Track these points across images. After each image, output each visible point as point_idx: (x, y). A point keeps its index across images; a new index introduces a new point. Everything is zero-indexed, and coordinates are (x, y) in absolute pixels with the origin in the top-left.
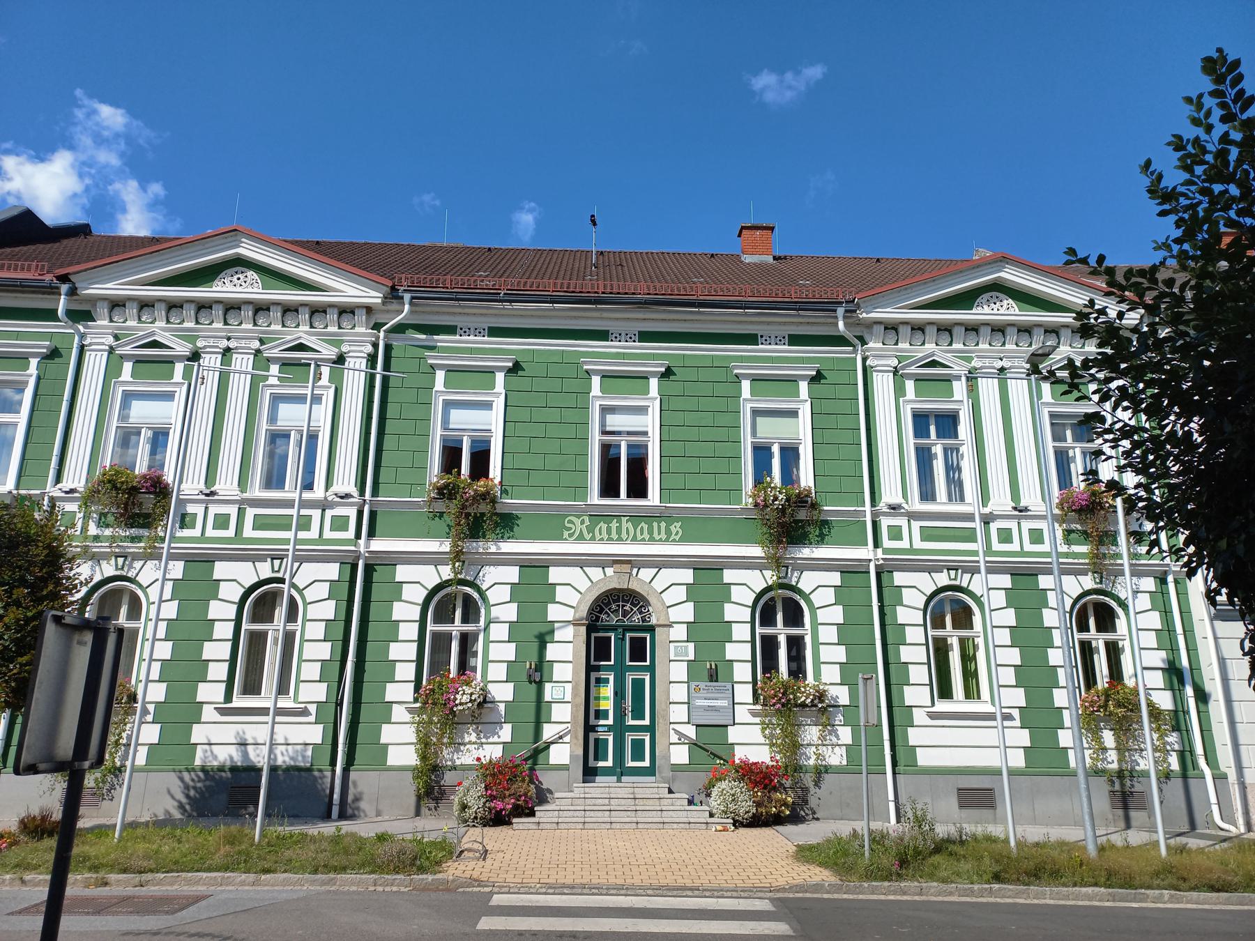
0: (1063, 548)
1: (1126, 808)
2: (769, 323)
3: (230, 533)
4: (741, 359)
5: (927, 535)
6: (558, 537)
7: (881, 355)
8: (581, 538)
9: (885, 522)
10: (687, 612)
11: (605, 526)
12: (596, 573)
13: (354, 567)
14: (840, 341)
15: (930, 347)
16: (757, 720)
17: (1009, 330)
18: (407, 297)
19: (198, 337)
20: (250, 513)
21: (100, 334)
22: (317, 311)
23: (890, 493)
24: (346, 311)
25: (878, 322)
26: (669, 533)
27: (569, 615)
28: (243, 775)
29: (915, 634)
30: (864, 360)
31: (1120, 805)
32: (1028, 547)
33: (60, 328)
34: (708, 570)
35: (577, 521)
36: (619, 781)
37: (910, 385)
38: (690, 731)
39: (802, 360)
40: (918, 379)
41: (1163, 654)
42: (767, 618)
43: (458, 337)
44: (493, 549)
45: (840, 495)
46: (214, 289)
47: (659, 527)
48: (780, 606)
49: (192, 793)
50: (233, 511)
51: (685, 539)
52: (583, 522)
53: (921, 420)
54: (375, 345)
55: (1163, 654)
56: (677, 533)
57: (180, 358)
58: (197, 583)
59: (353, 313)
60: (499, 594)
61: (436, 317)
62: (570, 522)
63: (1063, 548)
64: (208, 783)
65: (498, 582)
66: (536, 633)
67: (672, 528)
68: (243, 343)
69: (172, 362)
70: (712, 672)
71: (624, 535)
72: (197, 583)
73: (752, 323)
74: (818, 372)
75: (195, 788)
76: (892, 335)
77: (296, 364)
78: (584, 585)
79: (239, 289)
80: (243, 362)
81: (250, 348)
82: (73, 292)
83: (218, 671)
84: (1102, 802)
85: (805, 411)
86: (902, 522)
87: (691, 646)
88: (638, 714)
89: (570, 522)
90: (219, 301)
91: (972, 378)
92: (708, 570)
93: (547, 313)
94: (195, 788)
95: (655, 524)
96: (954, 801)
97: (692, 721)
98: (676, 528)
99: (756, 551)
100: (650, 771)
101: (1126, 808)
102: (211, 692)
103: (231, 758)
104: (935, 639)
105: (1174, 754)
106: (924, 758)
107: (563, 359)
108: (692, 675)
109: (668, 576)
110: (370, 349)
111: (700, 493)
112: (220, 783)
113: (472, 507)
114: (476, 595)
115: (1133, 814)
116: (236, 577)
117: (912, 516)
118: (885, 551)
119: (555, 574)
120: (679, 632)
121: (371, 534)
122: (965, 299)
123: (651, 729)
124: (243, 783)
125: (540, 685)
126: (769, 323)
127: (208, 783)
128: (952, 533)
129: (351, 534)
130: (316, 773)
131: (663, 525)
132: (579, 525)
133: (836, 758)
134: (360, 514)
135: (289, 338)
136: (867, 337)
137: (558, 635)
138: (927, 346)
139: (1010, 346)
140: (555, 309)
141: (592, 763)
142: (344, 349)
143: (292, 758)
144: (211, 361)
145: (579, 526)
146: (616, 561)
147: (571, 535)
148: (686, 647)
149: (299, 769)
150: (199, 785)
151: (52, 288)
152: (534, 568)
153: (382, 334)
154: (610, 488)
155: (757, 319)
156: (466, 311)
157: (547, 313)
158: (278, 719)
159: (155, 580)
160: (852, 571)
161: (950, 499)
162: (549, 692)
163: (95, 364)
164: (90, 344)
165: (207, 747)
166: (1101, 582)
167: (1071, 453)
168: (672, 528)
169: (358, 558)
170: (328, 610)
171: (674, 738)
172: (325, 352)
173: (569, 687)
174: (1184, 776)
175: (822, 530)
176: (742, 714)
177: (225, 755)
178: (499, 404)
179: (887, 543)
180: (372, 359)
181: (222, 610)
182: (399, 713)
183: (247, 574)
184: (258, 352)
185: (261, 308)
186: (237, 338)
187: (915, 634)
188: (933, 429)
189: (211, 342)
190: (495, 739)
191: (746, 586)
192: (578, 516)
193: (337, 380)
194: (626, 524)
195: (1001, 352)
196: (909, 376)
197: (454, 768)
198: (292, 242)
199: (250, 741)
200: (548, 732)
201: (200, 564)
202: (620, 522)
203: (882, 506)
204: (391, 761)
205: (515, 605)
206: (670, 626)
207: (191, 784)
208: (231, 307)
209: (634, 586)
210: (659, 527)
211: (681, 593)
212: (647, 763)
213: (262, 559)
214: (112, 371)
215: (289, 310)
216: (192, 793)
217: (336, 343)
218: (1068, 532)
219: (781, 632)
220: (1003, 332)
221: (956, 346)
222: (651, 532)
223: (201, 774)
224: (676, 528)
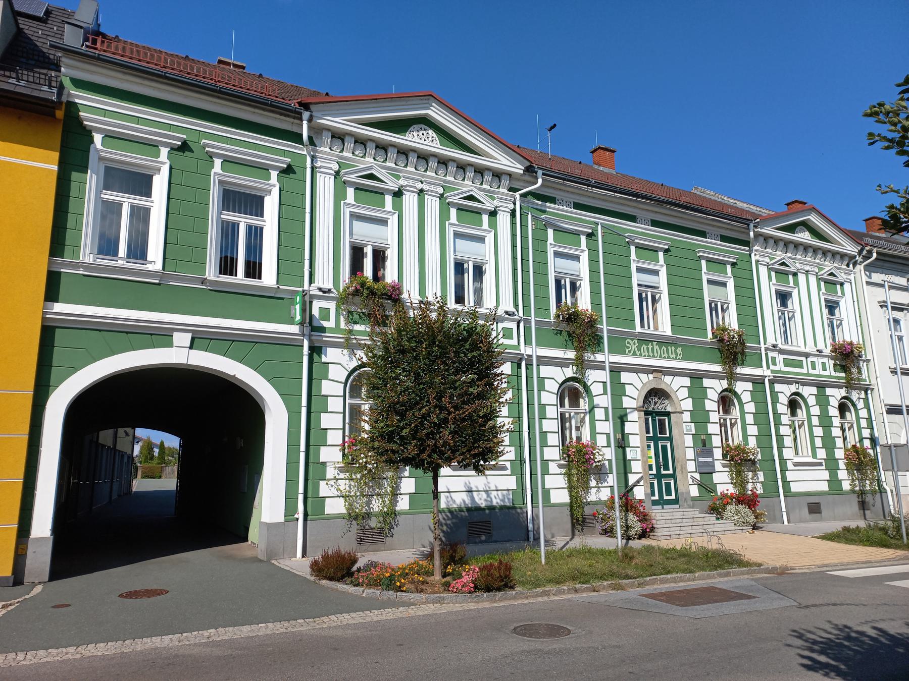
0: (833, 374)
1: (864, 510)
5: (787, 363)
6: (623, 353)
7: (328, 157)
8: (634, 354)
11: (650, 347)
12: (644, 377)
13: (519, 366)
15: (369, 160)
16: (728, 469)
17: (468, 169)
18: (540, 172)
22: (480, 171)
24: (498, 175)
25: (328, 129)
28: (475, 513)
29: (335, 404)
32: (811, 372)
34: (696, 377)
35: (632, 343)
36: (663, 508)
40: (358, 188)
44: (592, 358)
49: (445, 528)
51: (685, 358)
61: (608, 204)
63: (833, 374)
64: (454, 520)
65: (596, 378)
66: (618, 415)
68: (432, 188)
74: (289, 166)
75: (446, 524)
80: (432, 205)
81: (436, 192)
84: (855, 507)
85: (731, 284)
86: (775, 354)
87: (693, 425)
88: (667, 468)
91: (398, 194)
92: (696, 377)
93: (610, 199)
94: (446, 524)
96: (806, 510)
99: (718, 368)
100: (676, 502)
101: (864, 510)
103: (464, 502)
104: (352, 407)
106: (795, 488)
110: (512, 207)
112: (462, 519)
114: (581, 389)
115: (867, 512)
117: (782, 352)
118: (772, 371)
120: (687, 417)
122: (400, 126)
123: (673, 476)
124: (475, 520)
125: (624, 449)
126: (713, 226)
127: (454, 520)
129: (514, 342)
130: (519, 511)
135: (464, 189)
137: (630, 417)
138: (367, 159)
139: (410, 169)
140: (563, 184)
143: (501, 500)
144: (410, 201)
149: (509, 508)
150: (449, 522)
151: (296, 112)
152: (615, 371)
154: (227, 265)
155: (622, 201)
156: (568, 189)
157: (610, 199)
160: (758, 382)
162: (630, 453)
164: (320, 167)
165: (448, 494)
166: (576, 373)
167: (466, 266)
169: (521, 359)
171: (690, 482)
172: (487, 204)
173: (639, 450)
174: (881, 493)
176: (718, 466)
177: (460, 499)
179: (772, 367)
181: (711, 405)
182: (553, 467)
184: (442, 195)
186: (428, 183)
187: (335, 404)
190: (605, 484)
191: (714, 387)
192: (632, 340)
195: (423, 176)
196: (351, 184)
197: (588, 503)
199: (474, 489)
200: (632, 479)
204: (328, 510)
207: (443, 521)
209: (663, 387)
212: (673, 497)
215: (462, 167)
216: (445, 528)
218: (835, 365)
220: (446, 165)
221: (484, 186)
223: (449, 514)
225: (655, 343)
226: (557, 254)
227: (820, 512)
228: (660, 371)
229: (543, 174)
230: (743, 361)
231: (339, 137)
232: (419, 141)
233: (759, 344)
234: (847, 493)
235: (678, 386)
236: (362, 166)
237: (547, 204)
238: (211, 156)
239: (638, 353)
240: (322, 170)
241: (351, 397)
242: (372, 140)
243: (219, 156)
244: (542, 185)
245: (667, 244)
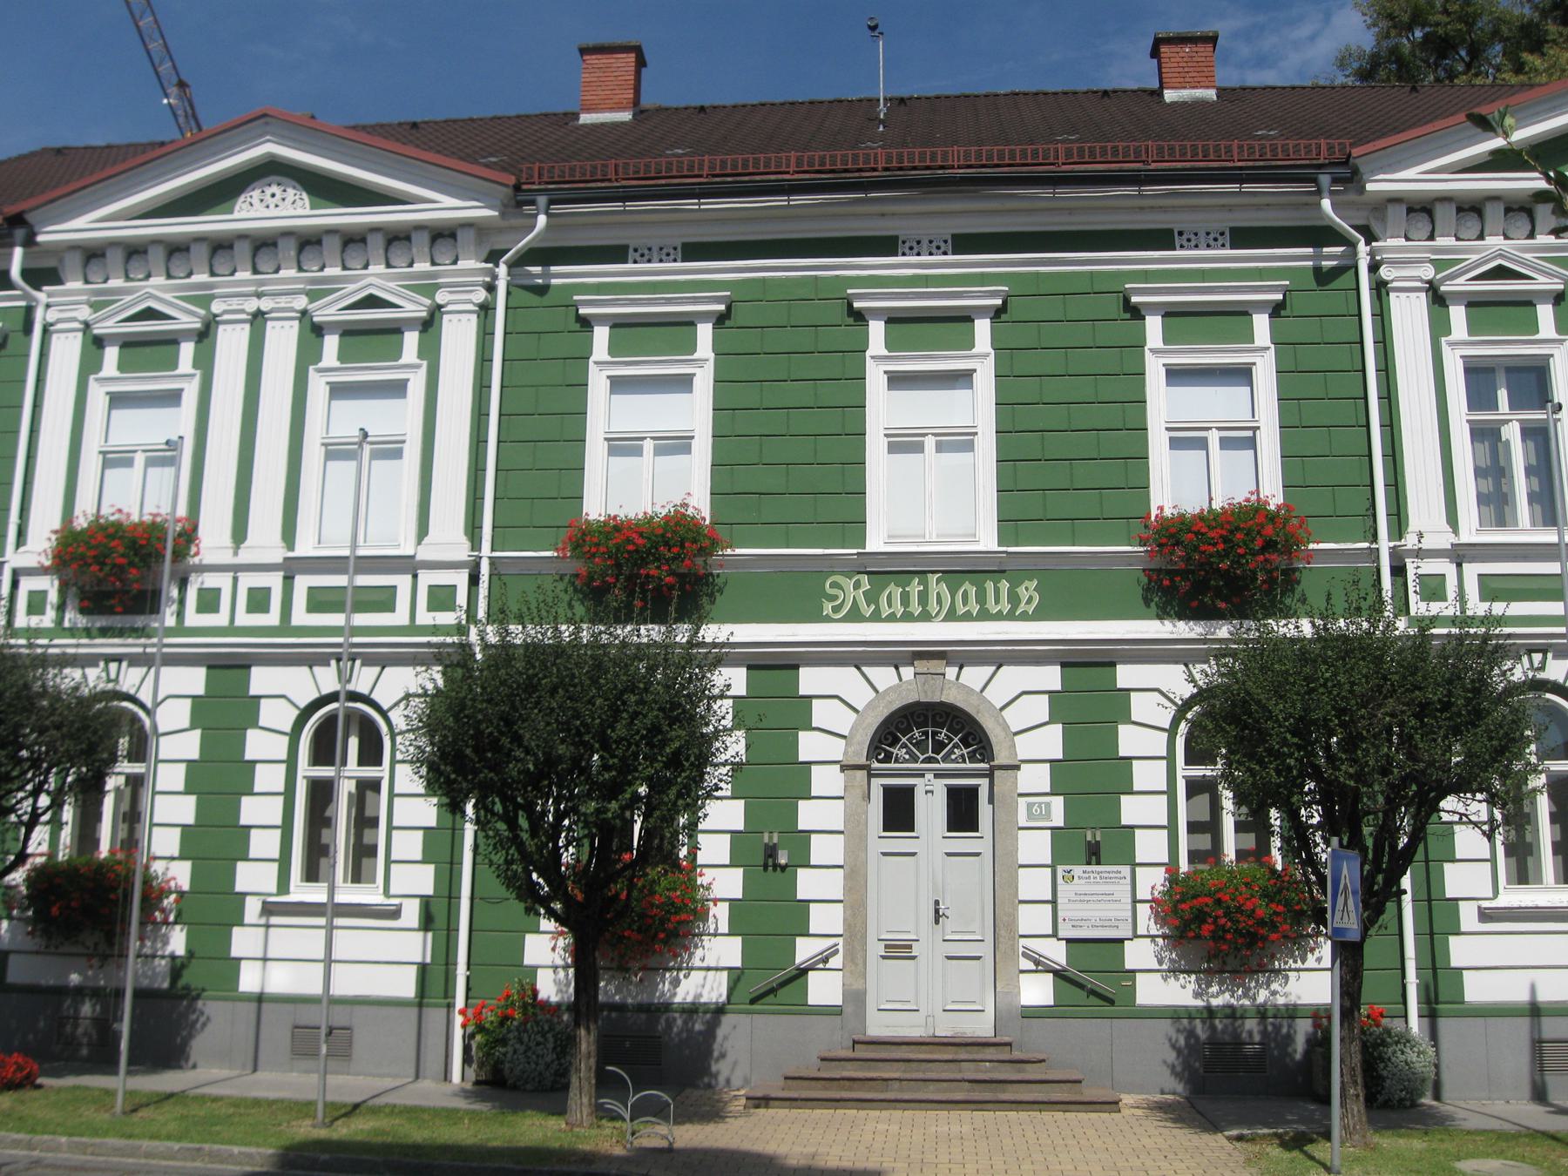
3: (272, 618)
4: (1146, 276)
6: (817, 617)
7: (1406, 259)
8: (854, 616)
10: (1051, 742)
12: (884, 677)
19: (213, 297)
20: (302, 583)
22: (397, 238)
23: (1426, 519)
24: (443, 235)
25: (1394, 199)
26: (1014, 599)
27: (836, 749)
30: (1374, 268)
35: (849, 584)
37: (1458, 314)
38: (1057, 953)
39: (1260, 274)
40: (1475, 303)
42: (324, 751)
43: (629, 266)
45: (1337, 523)
46: (236, 215)
47: (997, 591)
50: (274, 581)
52: (857, 586)
53: (1479, 375)
54: (491, 288)
56: (1030, 601)
57: (410, 323)
58: (226, 710)
59: (408, 238)
60: (173, 715)
62: (834, 585)
67: (1021, 590)
68: (283, 302)
71: (933, 607)
72: (226, 710)
76: (1473, 225)
77: (371, 336)
79: (273, 212)
80: (283, 340)
81: (292, 310)
83: (265, 844)
89: (834, 585)
90: (242, 236)
95: (990, 586)
97: (1061, 934)
98: (1028, 590)
106: (1476, 990)
107: (1093, 287)
108: (1061, 853)
109: (1014, 678)
110: (481, 295)
111: (1073, 527)
116: (283, 692)
119: (1126, 675)
120: (1035, 778)
126: (1174, 208)
128: (1534, 584)
131: (1005, 585)
132: (852, 590)
136: (1376, 228)
144: (232, 343)
145: (851, 593)
147: (836, 609)
148: (1048, 805)
152: (775, 667)
153: (502, 270)
155: (1293, 199)
158: (339, 921)
159: (171, 698)
161: (1533, 524)
163: (66, 352)
168: (1021, 590)
178: (704, 380)
183: (303, 685)
185: (308, 242)
188: (1503, 395)
189: (235, 303)
194: (936, 586)
196: (1458, 297)
198: (354, 128)
201: (228, 670)
202: (925, 583)
203: (1410, 541)
205: (198, 732)
208: (263, 245)
209: (951, 696)
210: (997, 591)
211: (1039, 708)
213: (323, 661)
214: (308, 354)
215: (353, 240)
217: (430, 290)
219: (352, 770)
222: (981, 598)
224: (1028, 590)
225: (933, 578)
226: (1176, 375)
228: (941, 656)
229: (1335, 181)
231: (92, 255)
232: (267, 213)
233: (1375, 538)
236: (1474, 257)
237: (554, 269)
238: (586, 323)
239: (868, 611)
240: (59, 326)
241: (1190, 760)
242: (1494, 197)
243: (877, 313)
244: (548, 226)
245: (717, 300)
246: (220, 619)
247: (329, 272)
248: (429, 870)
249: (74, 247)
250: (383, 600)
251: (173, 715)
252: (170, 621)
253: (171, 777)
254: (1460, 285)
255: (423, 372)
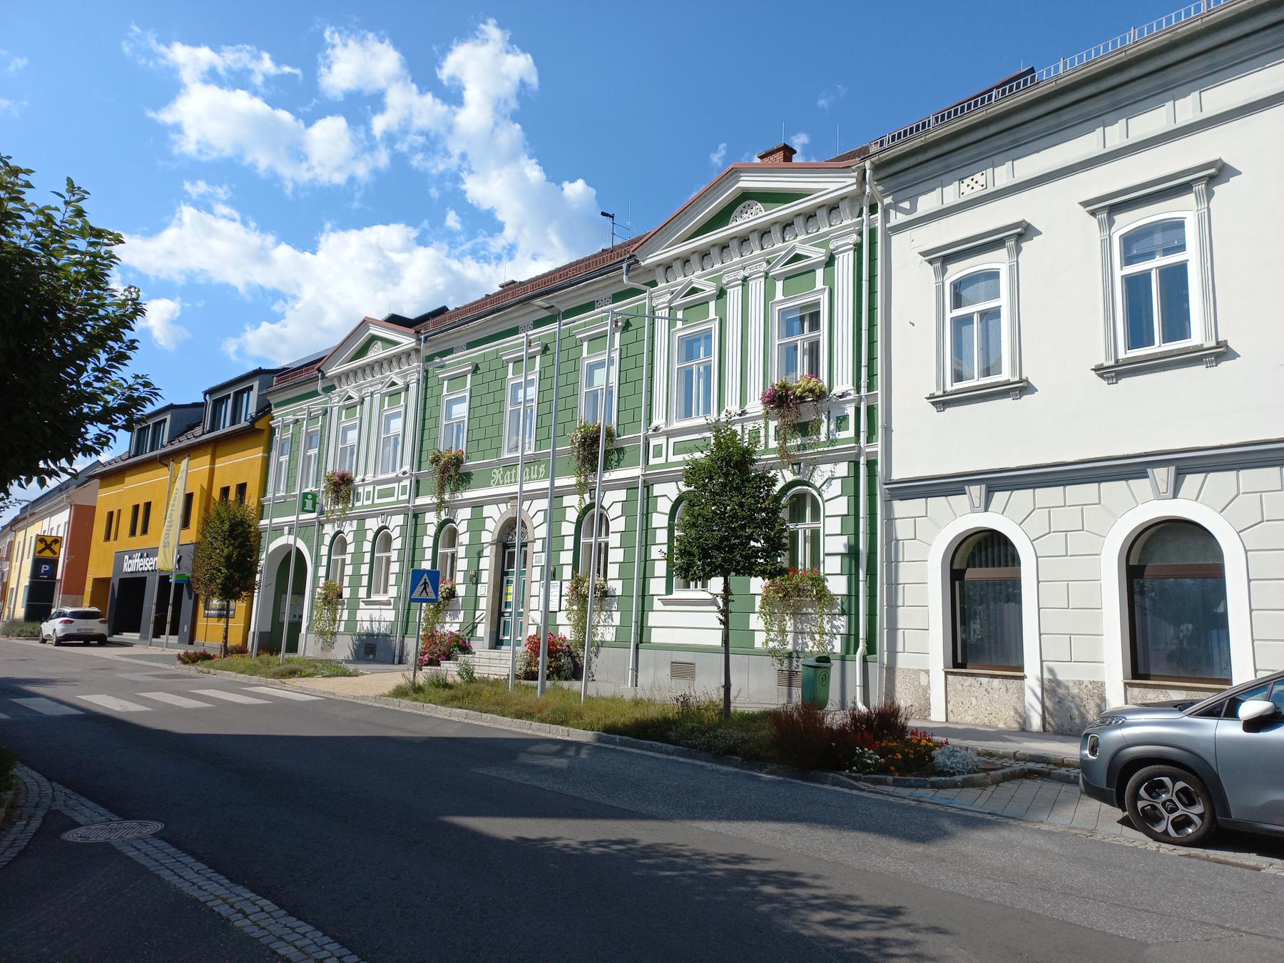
2: (597, 290)
6: (489, 485)
8: (498, 484)
9: (653, 442)
12: (503, 507)
13: (857, 464)
14: (633, 292)
21: (661, 297)
24: (832, 207)
31: (786, 682)
33: (321, 399)
41: (844, 539)
48: (592, 519)
54: (860, 234)
55: (844, 539)
57: (818, 265)
60: (615, 511)
65: (613, 501)
69: (814, 271)
70: (552, 573)
73: (588, 293)
78: (497, 516)
80: (757, 287)
82: (323, 376)
92: (556, 495)
96: (668, 671)
102: (362, 593)
105: (839, 637)
106: (657, 637)
110: (854, 238)
113: (453, 473)
121: (417, 495)
126: (597, 290)
133: (609, 635)
134: (858, 410)
141: (501, 637)
142: (831, 247)
144: (734, 295)
146: (511, 498)
152: (477, 506)
160: (630, 486)
170: (841, 506)
175: (616, 456)
180: (858, 247)
191: (572, 504)
193: (829, 281)
206: (534, 541)
215: (786, 225)
227: (693, 678)
230: (619, 461)
231: (667, 266)
234: (759, 653)
235: (536, 511)
246: (661, 460)
247: (822, 231)
248: (844, 579)
249: (659, 265)
250: (390, 493)
251: (615, 511)
252: (823, 438)
253: (833, 526)
254: (778, 270)
255: (826, 293)
